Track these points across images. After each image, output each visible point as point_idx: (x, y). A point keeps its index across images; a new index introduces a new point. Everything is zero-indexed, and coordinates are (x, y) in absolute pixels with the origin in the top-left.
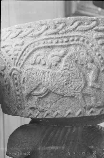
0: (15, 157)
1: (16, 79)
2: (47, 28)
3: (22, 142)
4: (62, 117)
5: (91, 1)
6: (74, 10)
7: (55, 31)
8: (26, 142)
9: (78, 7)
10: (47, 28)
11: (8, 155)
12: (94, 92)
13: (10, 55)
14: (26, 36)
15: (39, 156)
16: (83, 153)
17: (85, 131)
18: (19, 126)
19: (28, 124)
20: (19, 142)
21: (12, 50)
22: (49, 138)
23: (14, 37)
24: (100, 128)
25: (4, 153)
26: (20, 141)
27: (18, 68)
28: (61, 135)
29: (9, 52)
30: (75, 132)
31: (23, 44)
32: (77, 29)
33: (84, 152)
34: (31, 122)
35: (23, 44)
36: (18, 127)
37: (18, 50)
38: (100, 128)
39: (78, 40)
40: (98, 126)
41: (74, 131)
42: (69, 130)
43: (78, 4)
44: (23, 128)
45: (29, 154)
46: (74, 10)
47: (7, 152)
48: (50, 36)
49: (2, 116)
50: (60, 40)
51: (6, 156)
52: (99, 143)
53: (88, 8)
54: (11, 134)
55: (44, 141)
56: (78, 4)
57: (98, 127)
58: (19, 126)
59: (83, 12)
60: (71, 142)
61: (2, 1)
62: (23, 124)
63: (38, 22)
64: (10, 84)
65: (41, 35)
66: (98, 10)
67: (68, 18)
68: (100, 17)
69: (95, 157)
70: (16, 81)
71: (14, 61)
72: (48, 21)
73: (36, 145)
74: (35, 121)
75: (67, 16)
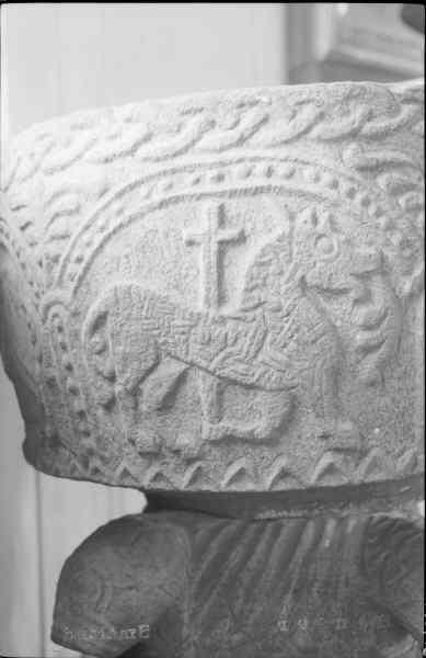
3: (115, 588)
5: (396, 7)
6: (323, 45)
7: (235, 134)
8: (131, 588)
11: (56, 639)
12: (395, 383)
14: (79, 157)
18: (104, 521)
19: (139, 515)
20: (103, 587)
22: (227, 572)
26: (108, 584)
27: (66, 294)
28: (274, 561)
29: (30, 230)
30: (331, 545)
36: (94, 528)
42: (331, 525)
44: (115, 532)
45: (144, 634)
46: (323, 45)
47: (54, 628)
48: (160, 167)
49: (31, 484)
54: (69, 552)
55: (203, 583)
59: (362, 55)
60: (314, 589)
61: (423, 7)
62: (117, 516)
63: (182, 100)
64: (50, 352)
65: (226, 143)
68: (166, 101)
72: (271, 89)
74: (159, 501)
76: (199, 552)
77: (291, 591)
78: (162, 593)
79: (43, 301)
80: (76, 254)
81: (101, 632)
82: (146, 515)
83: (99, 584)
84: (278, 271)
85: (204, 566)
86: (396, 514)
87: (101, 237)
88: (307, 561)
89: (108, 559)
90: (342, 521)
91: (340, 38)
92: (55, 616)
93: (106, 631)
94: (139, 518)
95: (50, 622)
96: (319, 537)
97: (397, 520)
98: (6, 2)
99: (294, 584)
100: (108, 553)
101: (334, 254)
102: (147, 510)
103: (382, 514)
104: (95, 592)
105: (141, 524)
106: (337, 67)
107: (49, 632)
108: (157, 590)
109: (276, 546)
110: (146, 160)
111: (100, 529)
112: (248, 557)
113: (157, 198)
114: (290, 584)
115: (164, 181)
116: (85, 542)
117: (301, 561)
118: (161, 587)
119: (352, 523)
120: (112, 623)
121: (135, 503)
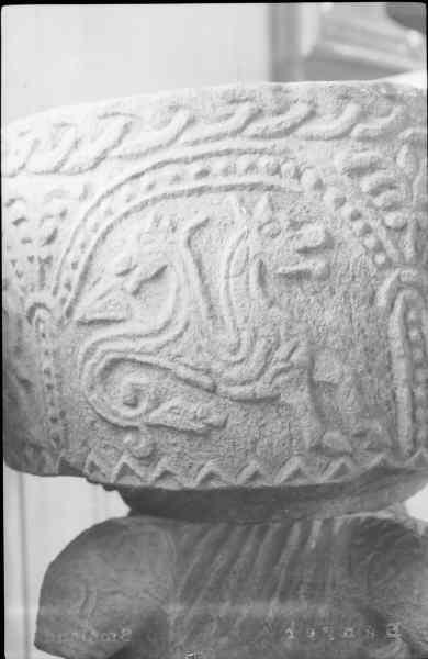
0: (69, 653)
2: (191, 122)
4: (225, 485)
6: (307, 41)
8: (114, 593)
10: (191, 122)
11: (40, 646)
13: (26, 241)
15: (171, 650)
16: (349, 633)
18: (88, 524)
19: (124, 518)
20: (88, 592)
21: (34, 217)
23: (48, 172)
25: (27, 637)
26: (93, 589)
28: (260, 562)
29: (23, 226)
33: (351, 630)
42: (317, 525)
43: (323, 18)
44: (101, 534)
45: (125, 638)
46: (307, 41)
47: (38, 634)
50: (218, 164)
51: (33, 647)
52: (416, 592)
53: (364, 32)
54: (53, 558)
58: (88, 527)
59: (347, 51)
61: (423, 6)
62: (102, 519)
63: (103, 105)
69: (401, 649)
73: (158, 603)
74: (142, 501)
76: (186, 553)
77: (277, 594)
78: (147, 596)
79: (29, 303)
80: (70, 258)
81: (85, 632)
82: (131, 519)
83: (83, 588)
84: (133, 402)
85: (189, 571)
86: (383, 515)
87: (95, 237)
88: (292, 565)
89: (94, 563)
90: (328, 523)
91: (324, 34)
92: (38, 623)
93: (88, 634)
94: (124, 523)
95: (33, 629)
96: (304, 541)
97: (385, 521)
98: (8, 4)
99: (279, 587)
100: (93, 556)
101: (239, 357)
102: (131, 514)
103: (369, 514)
104: (79, 598)
105: (125, 527)
106: (323, 65)
107: (32, 642)
108: (142, 595)
109: (262, 547)
110: (255, 137)
111: (83, 534)
112: (232, 561)
113: (141, 198)
114: (276, 585)
115: (196, 167)
116: (79, 538)
117: (287, 562)
118: (146, 591)
119: (338, 524)
120: (97, 628)
121: (117, 508)
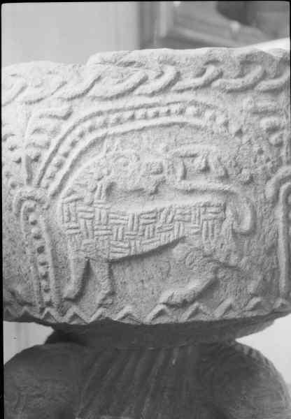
1: (34, 223)
4: (131, 322)
6: (163, 28)
9: (177, 20)
17: (204, 360)
24: (246, 352)
30: (176, 362)
31: (67, 116)
32: (91, 93)
34: (51, 340)
35: (67, 116)
37: (87, 132)
38: (246, 352)
39: (182, 112)
40: (237, 344)
41: (174, 362)
43: (174, 11)
46: (163, 28)
56: (174, 11)
57: (243, 349)
59: (190, 33)
66: (230, 29)
67: (146, 52)
70: (34, 230)
71: (30, 171)
75: (145, 43)
91: (176, 23)
118: (60, 395)
